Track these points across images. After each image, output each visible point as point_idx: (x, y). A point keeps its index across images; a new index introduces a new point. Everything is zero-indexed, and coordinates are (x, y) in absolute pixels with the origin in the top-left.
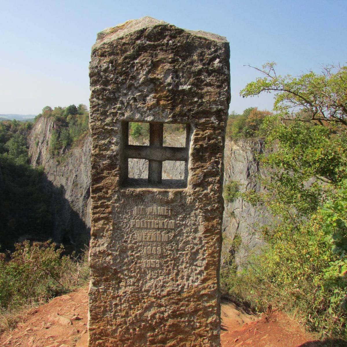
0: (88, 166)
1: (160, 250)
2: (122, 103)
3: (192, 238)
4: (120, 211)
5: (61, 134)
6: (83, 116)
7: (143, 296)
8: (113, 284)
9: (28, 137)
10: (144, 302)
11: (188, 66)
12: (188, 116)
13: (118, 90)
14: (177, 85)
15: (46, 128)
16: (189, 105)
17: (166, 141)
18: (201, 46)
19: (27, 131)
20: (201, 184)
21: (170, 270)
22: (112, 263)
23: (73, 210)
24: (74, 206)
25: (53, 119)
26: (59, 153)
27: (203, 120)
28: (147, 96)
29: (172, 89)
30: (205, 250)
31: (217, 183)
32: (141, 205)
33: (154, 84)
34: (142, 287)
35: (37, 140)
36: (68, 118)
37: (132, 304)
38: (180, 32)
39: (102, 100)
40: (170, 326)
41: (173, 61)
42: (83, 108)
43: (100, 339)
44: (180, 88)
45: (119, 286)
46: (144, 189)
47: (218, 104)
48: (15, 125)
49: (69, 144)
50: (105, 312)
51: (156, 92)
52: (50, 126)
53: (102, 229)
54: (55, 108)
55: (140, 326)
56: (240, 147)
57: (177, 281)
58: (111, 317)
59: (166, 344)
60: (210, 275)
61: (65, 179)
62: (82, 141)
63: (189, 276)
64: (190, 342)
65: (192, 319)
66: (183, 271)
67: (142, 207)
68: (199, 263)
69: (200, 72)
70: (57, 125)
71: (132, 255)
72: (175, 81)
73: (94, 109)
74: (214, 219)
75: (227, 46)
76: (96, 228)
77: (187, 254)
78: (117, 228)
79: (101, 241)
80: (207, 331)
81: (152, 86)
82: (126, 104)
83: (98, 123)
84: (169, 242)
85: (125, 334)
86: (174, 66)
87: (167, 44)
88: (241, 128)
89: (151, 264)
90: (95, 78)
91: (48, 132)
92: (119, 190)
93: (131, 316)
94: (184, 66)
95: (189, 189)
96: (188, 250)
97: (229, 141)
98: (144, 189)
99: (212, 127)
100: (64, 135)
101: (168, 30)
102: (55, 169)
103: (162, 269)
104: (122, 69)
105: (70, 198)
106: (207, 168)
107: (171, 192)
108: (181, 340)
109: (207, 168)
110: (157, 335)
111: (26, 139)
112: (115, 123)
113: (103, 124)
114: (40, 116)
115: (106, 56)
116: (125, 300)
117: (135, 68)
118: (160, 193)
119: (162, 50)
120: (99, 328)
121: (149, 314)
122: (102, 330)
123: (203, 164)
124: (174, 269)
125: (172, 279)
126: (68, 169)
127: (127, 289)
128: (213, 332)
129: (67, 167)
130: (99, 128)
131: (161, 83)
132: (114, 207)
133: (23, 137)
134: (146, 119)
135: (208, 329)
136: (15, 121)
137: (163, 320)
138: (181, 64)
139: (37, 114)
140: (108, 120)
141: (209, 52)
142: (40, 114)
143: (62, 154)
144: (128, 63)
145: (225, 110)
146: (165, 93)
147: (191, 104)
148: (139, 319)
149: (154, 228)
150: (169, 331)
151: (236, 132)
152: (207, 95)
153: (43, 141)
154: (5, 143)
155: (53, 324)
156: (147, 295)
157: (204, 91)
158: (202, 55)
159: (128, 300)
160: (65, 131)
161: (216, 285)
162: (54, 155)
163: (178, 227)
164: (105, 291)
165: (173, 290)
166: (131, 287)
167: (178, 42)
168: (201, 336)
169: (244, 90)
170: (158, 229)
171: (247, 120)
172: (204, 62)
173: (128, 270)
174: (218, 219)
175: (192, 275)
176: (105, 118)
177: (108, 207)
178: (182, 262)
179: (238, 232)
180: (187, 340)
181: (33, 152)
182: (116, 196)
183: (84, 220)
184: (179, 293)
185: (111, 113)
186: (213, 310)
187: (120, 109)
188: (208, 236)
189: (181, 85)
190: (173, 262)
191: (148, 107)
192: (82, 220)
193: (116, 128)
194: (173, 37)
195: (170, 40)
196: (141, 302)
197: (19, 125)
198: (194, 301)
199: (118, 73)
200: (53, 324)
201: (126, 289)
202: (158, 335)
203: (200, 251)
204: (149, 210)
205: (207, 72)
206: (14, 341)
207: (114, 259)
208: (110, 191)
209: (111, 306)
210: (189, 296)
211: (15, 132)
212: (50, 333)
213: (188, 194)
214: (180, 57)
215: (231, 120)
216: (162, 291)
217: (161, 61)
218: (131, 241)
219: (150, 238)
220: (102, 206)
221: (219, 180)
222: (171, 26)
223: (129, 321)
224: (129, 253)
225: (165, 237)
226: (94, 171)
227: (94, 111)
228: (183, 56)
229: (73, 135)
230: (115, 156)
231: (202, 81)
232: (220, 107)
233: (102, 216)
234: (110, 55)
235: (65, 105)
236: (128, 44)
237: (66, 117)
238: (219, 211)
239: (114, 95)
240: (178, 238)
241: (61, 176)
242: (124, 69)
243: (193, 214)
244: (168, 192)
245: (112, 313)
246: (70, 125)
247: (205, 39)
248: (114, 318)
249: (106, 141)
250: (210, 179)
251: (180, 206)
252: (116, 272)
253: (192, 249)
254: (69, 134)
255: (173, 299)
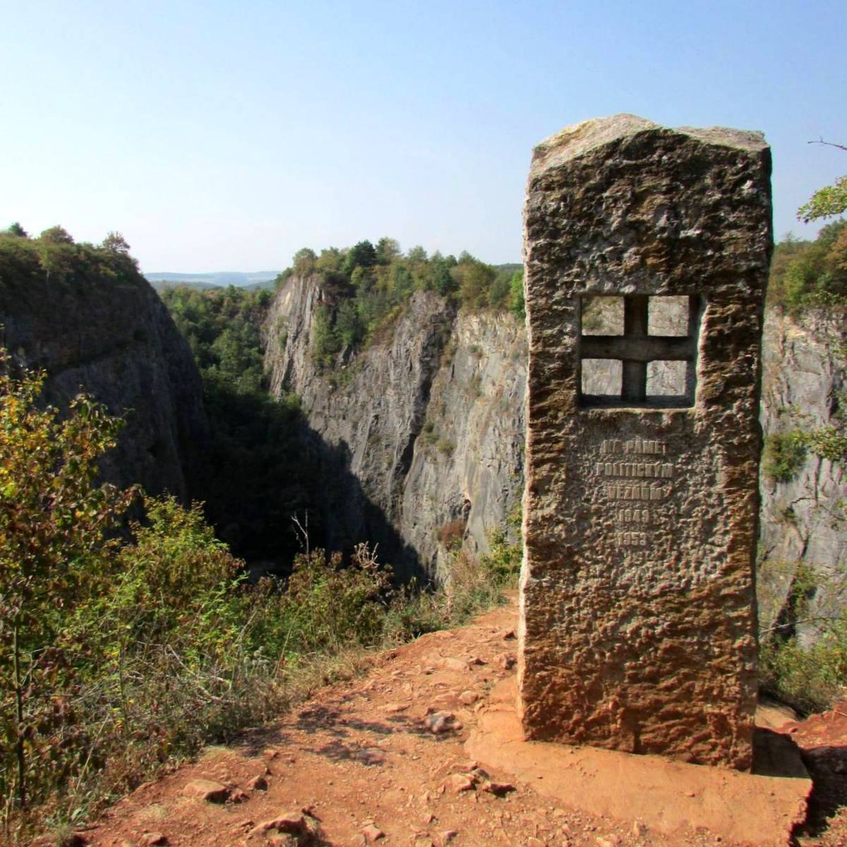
0: (404, 392)
1: (648, 516)
2: (582, 265)
3: (704, 495)
4: (579, 448)
5: (338, 315)
6: (388, 267)
7: (617, 596)
8: (565, 574)
9: (262, 326)
10: (620, 607)
11: (696, 197)
12: (696, 282)
13: (575, 244)
14: (677, 231)
15: (302, 302)
16: (697, 263)
17: (601, 321)
18: (719, 160)
19: (260, 312)
20: (719, 399)
21: (665, 551)
22: (564, 535)
23: (369, 501)
24: (371, 491)
25: (318, 278)
26: (334, 361)
27: (723, 288)
28: (624, 251)
29: (668, 238)
30: (728, 517)
31: (750, 396)
32: (615, 437)
33: (636, 231)
34: (615, 580)
35: (282, 332)
36: (353, 276)
37: (597, 610)
38: (681, 139)
39: (548, 262)
40: (666, 651)
41: (670, 190)
42: (390, 248)
43: (542, 669)
44: (682, 234)
45: (576, 577)
46: (619, 410)
47: (751, 258)
48: (233, 298)
49: (358, 342)
50: (551, 622)
51: (640, 243)
52: (313, 297)
53: (548, 479)
54: (324, 252)
55: (613, 648)
56: (807, 330)
57: (678, 570)
58: (562, 631)
59: (658, 683)
60: (738, 561)
61: (350, 425)
62: (389, 332)
63: (699, 563)
64: (701, 683)
65: (706, 639)
66: (688, 554)
67: (616, 440)
68: (717, 539)
69: (717, 205)
70: (328, 293)
71: (598, 524)
72: (672, 224)
73: (535, 278)
74: (744, 460)
75: (766, 155)
76: (537, 477)
77: (695, 523)
78: (573, 478)
79: (545, 499)
80: (734, 663)
81: (632, 234)
82: (588, 267)
83: (542, 301)
84: (663, 501)
85: (586, 662)
86: (671, 199)
87: (659, 161)
88: (810, 279)
89: (631, 540)
90: (536, 227)
91: (308, 312)
92: (576, 413)
93: (596, 630)
94: (688, 198)
95: (698, 409)
96: (696, 516)
97: (778, 315)
98: (619, 410)
99: (739, 299)
100: (345, 317)
101: (660, 138)
102: (326, 402)
103: (652, 550)
104: (581, 209)
105: (362, 473)
106: (731, 371)
107: (666, 415)
108: (687, 677)
109: (731, 371)
110: (642, 667)
111: (257, 331)
112: (571, 299)
113: (550, 302)
114: (289, 273)
115: (554, 189)
116: (587, 602)
117: (604, 206)
118: (647, 415)
119: (649, 172)
120: (541, 649)
121: (628, 628)
122: (546, 653)
123: (723, 364)
124: (671, 549)
125: (669, 568)
126: (356, 402)
127: (589, 582)
128: (744, 666)
129: (353, 395)
130: (543, 309)
131: (649, 229)
132: (567, 442)
133: (250, 328)
134: (622, 290)
135: (734, 659)
136: (232, 288)
137: (652, 640)
138: (684, 193)
139: (282, 269)
140: (558, 295)
141: (734, 169)
142: (288, 269)
143: (343, 364)
144: (592, 199)
145: (762, 268)
146: (655, 244)
147: (704, 260)
148: (612, 636)
149: (636, 477)
150: (664, 660)
151: (796, 289)
152: (730, 245)
153: (298, 333)
154: (211, 343)
155: (436, 668)
156: (624, 594)
157: (724, 237)
158: (720, 176)
159: (592, 602)
160: (348, 308)
161: (749, 580)
162: (322, 367)
163: (680, 475)
164: (552, 587)
165: (671, 586)
166: (596, 580)
167: (679, 157)
168: (722, 671)
169: (807, 207)
170: (644, 478)
171: (830, 257)
172: (724, 188)
173: (592, 549)
174: (751, 461)
175: (705, 561)
176: (553, 293)
177: (557, 441)
178: (688, 537)
179: (804, 564)
180: (695, 679)
181: (275, 361)
182: (572, 422)
183: (396, 526)
184: (682, 592)
185: (562, 284)
186: (744, 625)
187: (578, 275)
188: (734, 492)
189: (684, 228)
190: (670, 537)
191: (626, 270)
192: (390, 527)
193: (572, 308)
194: (668, 149)
195: (665, 154)
196: (613, 605)
197: (242, 298)
198: (709, 608)
199: (576, 216)
200: (436, 668)
201: (587, 583)
202: (644, 667)
203: (719, 518)
204: (627, 445)
205: (729, 205)
206: (380, 686)
207: (569, 530)
208: (560, 414)
209: (562, 611)
210: (700, 598)
211: (232, 314)
212: (434, 680)
213: (696, 417)
214: (682, 182)
215: (783, 257)
216: (652, 587)
217: (649, 192)
218: (597, 499)
219: (630, 494)
220: (548, 439)
221: (752, 392)
222: (666, 131)
223: (594, 638)
224: (594, 520)
225: (655, 491)
226: (535, 381)
227: (535, 282)
228: (688, 180)
229: (367, 316)
230: (569, 354)
231: (721, 220)
232: (753, 264)
233: (548, 456)
234: (561, 186)
235: (346, 243)
236: (592, 167)
237: (349, 274)
238: (754, 447)
239: (569, 254)
240: (679, 494)
241: (341, 420)
242: (585, 209)
243: (705, 452)
244: (661, 414)
245: (564, 625)
246: (358, 292)
247: (726, 148)
248: (567, 633)
249: (555, 331)
250: (737, 391)
251: (681, 438)
252: (571, 553)
253: (704, 515)
254: (357, 314)
255: (670, 601)
